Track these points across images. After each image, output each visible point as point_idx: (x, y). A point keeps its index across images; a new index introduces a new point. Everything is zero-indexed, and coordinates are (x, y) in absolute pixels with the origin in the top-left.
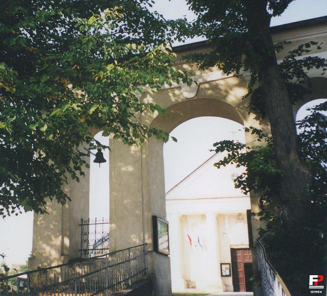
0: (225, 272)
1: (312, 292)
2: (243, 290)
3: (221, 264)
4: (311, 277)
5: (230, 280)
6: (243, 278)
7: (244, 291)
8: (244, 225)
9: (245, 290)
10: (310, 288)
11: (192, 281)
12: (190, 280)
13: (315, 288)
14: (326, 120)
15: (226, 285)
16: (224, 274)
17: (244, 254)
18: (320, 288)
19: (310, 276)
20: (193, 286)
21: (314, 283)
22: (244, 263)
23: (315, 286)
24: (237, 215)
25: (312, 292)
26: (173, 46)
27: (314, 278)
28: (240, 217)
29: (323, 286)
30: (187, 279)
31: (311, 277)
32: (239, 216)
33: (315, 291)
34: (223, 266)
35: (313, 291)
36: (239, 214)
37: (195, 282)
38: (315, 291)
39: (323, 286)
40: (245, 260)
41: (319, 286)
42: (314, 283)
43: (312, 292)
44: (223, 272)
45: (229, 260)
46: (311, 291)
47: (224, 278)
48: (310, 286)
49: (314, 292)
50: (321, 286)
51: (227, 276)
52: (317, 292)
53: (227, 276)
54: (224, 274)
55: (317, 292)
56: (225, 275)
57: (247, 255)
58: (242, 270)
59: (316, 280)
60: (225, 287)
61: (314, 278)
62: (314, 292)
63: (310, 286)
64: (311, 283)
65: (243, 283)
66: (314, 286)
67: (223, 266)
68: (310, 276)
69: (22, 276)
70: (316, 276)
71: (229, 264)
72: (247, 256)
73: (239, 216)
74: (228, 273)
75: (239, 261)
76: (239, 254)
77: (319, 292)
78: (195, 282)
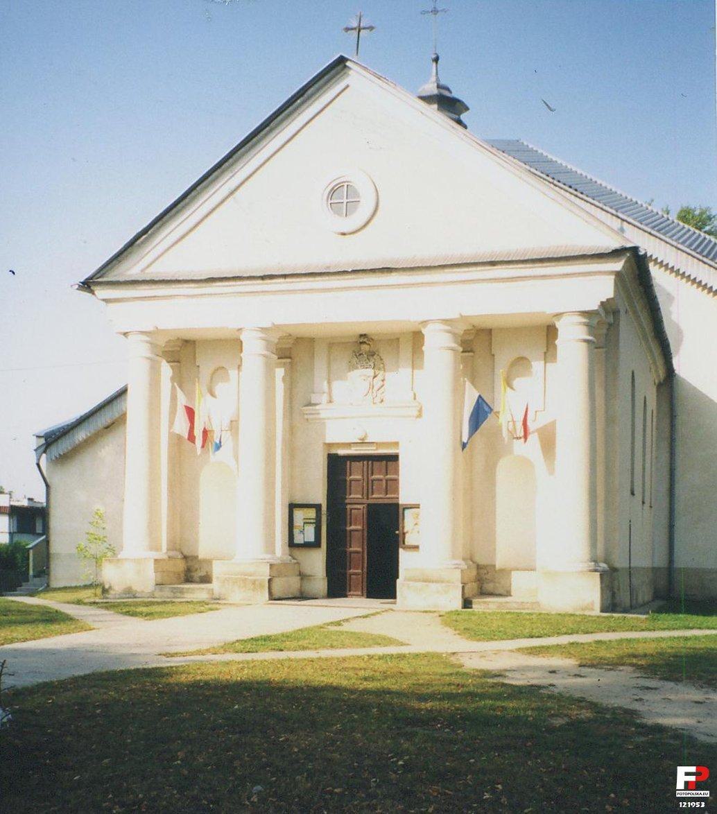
0: (302, 532)
1: (683, 805)
2: (360, 593)
3: (292, 507)
4: (681, 770)
5: (316, 562)
6: (363, 552)
7: (363, 595)
8: (375, 377)
9: (365, 591)
10: (679, 796)
11: (201, 556)
12: (196, 557)
13: (689, 796)
14: (708, 563)
15: (303, 576)
16: (299, 539)
17: (372, 474)
18: (700, 796)
19: (678, 767)
20: (203, 574)
21: (687, 783)
22: (369, 505)
23: (689, 790)
24: (354, 340)
25: (683, 805)
26: (513, 573)
27: (687, 774)
28: (365, 348)
29: (708, 792)
30: (186, 553)
31: (681, 770)
32: (361, 343)
33: (689, 803)
34: (299, 515)
35: (685, 803)
36: (361, 336)
37: (209, 562)
38: (689, 803)
39: (708, 792)
40: (373, 494)
41: (699, 792)
42: (687, 783)
43: (683, 805)
44: (296, 532)
45: (318, 494)
46: (681, 803)
47: (297, 553)
48: (677, 792)
49: (687, 805)
50: (702, 792)
51: (307, 545)
52: (693, 804)
53: (307, 545)
54: (299, 539)
55: (693, 804)
56: (302, 542)
57: (381, 477)
58: (359, 527)
59: (693, 778)
60: (299, 582)
61: (687, 774)
62: (687, 805)
63: (677, 792)
64: (680, 785)
65: (357, 572)
66: (688, 792)
67: (299, 515)
68: (678, 767)
69: (22, 597)
70: (693, 769)
71: (318, 507)
72: (381, 480)
73: (361, 343)
74: (310, 535)
75: (354, 496)
76: (355, 474)
77: (699, 806)
78: (209, 562)
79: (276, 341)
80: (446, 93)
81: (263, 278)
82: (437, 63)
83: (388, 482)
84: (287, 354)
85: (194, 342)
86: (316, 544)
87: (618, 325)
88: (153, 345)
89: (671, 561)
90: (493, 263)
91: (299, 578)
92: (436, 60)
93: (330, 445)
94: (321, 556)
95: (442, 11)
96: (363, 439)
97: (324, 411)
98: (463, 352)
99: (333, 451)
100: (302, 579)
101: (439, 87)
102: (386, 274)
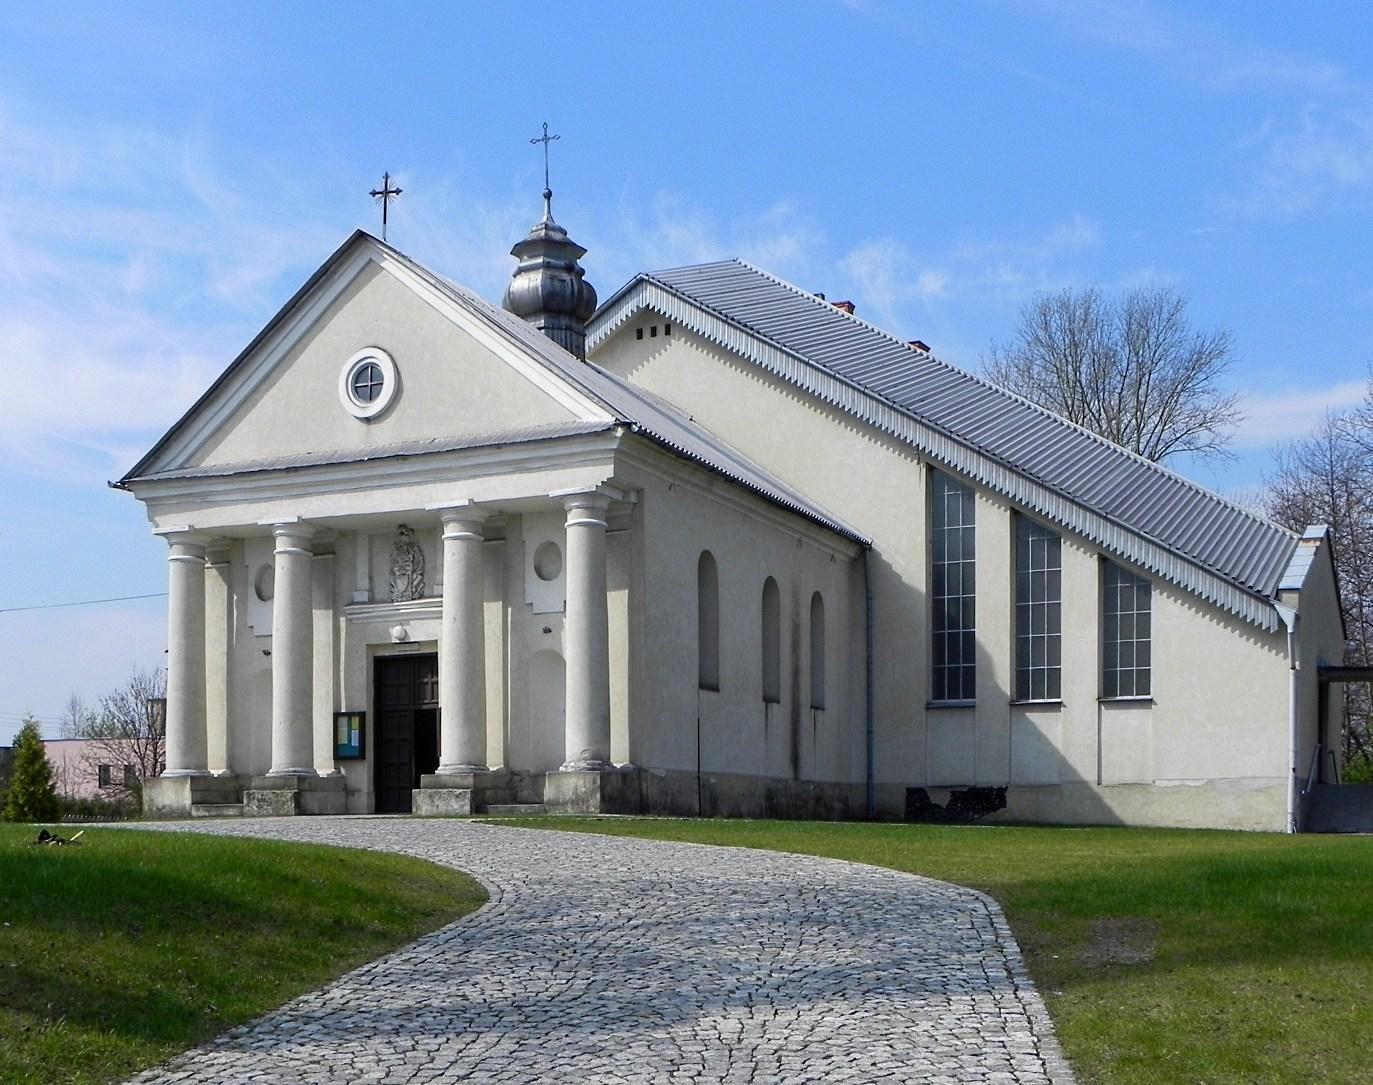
36: (401, 526)
71: (362, 715)
79: (483, 520)
80: (558, 236)
81: (288, 470)
82: (549, 200)
83: (1336, 689)
84: (331, 550)
85: (243, 539)
86: (362, 756)
87: (642, 505)
88: (188, 547)
89: (870, 776)
90: (498, 446)
91: (343, 793)
92: (548, 196)
93: (370, 647)
94: (366, 769)
95: (554, 138)
96: (403, 639)
97: (324, 612)
98: (485, 541)
99: (381, 653)
100: (347, 796)
101: (547, 227)
102: (401, 462)
